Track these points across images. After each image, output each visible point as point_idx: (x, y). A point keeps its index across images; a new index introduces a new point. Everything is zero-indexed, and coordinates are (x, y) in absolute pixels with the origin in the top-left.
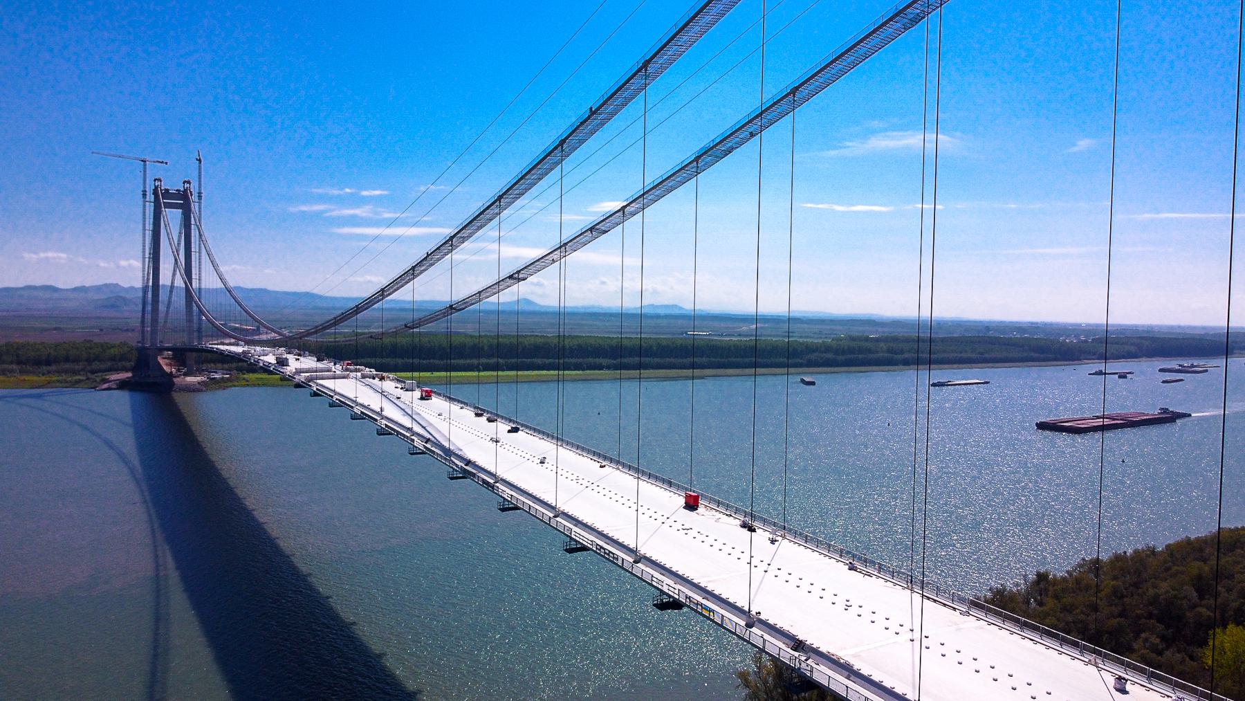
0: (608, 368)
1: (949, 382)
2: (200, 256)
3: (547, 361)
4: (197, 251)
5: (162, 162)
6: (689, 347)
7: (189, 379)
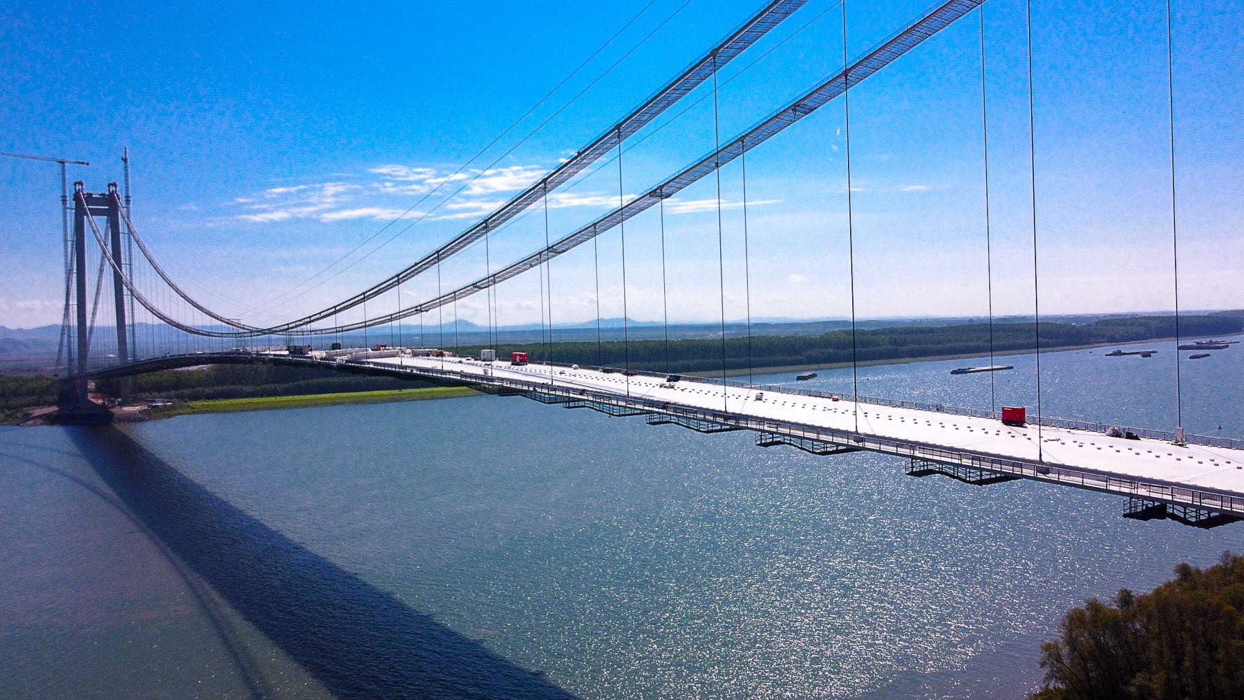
1: (970, 368)
4: (128, 263)
5: (83, 163)
7: (125, 409)
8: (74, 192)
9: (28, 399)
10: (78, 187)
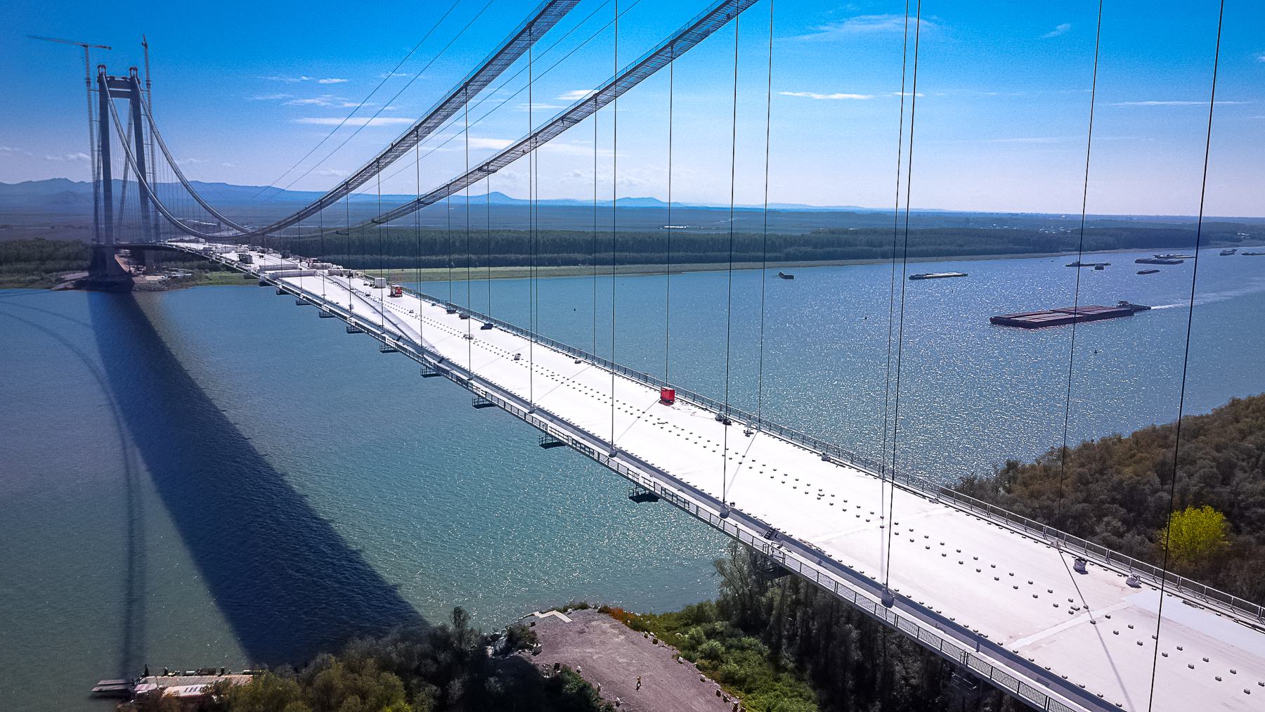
0: (584, 263)
4: (149, 143)
7: (149, 278)
8: (98, 75)
9: (63, 263)
10: (102, 70)
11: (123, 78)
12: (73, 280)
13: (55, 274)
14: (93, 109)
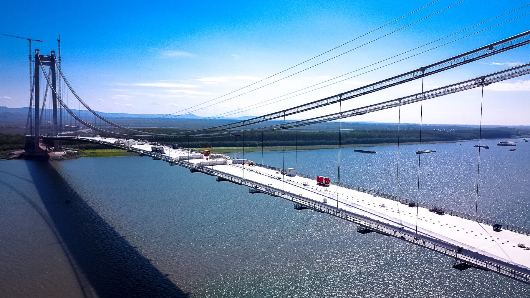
0: (259, 145)
2: (60, 90)
3: (231, 142)
5: (39, 41)
6: (295, 136)
7: (57, 153)
11: (47, 56)
12: (18, 154)
13: (8, 151)
14: (32, 67)
